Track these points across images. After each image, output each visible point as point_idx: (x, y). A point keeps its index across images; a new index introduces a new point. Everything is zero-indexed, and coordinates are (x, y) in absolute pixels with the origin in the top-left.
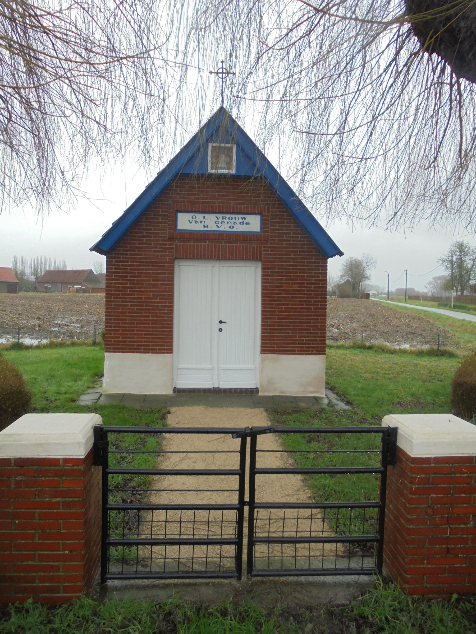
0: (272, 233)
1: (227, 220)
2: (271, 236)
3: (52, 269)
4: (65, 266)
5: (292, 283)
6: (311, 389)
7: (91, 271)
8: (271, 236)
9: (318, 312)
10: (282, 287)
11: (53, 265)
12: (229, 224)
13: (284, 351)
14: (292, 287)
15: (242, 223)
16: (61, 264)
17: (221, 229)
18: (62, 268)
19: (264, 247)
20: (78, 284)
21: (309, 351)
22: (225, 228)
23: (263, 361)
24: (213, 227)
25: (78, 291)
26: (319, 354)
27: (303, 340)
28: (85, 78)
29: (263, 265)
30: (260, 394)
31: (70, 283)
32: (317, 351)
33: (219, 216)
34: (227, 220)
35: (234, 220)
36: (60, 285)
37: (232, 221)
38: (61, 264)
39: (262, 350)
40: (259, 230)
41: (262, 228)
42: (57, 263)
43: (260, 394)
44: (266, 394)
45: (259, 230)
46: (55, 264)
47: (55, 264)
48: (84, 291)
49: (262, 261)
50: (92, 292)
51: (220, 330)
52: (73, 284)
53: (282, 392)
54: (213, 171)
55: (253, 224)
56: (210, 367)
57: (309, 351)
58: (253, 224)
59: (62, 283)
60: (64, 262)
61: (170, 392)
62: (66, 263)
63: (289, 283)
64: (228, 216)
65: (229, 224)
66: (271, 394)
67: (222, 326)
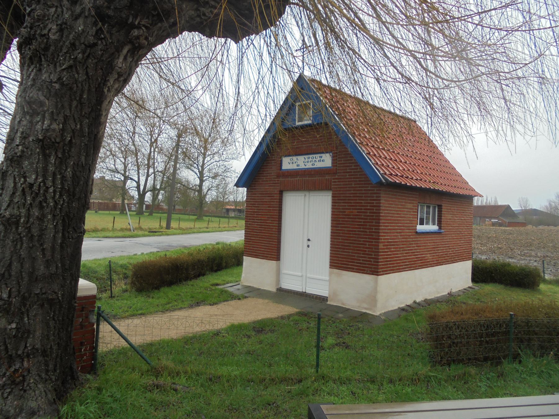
0: (339, 167)
1: (311, 159)
2: (339, 170)
3: (484, 204)
4: (496, 201)
5: (353, 209)
6: (365, 305)
7: (508, 207)
8: (339, 170)
9: (372, 235)
10: (345, 212)
11: (485, 201)
12: (312, 163)
13: (338, 267)
14: (352, 212)
15: (319, 161)
16: (493, 200)
17: (307, 167)
18: (493, 204)
19: (334, 179)
20: (495, 218)
21: (365, 270)
22: (309, 166)
23: (331, 274)
24: (302, 166)
25: (494, 224)
26: (373, 274)
27: (360, 260)
28: (508, 25)
29: (333, 194)
30: (328, 303)
31: (487, 217)
32: (371, 271)
33: (306, 157)
34: (311, 159)
35: (315, 159)
36: (479, 218)
37: (314, 160)
38: (493, 200)
39: (330, 265)
40: (331, 166)
41: (332, 163)
42: (489, 199)
43: (328, 303)
44: (332, 303)
45: (331, 166)
46: (487, 200)
47: (487, 200)
48: (500, 225)
49: (333, 191)
50: (508, 226)
51: (308, 246)
52: (491, 218)
53: (343, 304)
54: (300, 123)
55: (325, 161)
56: (300, 274)
57: (365, 270)
58: (325, 161)
59: (480, 217)
60: (496, 199)
61: (274, 290)
62: (498, 199)
63: (350, 209)
64: (311, 156)
65: (312, 163)
66: (335, 304)
67: (309, 243)
